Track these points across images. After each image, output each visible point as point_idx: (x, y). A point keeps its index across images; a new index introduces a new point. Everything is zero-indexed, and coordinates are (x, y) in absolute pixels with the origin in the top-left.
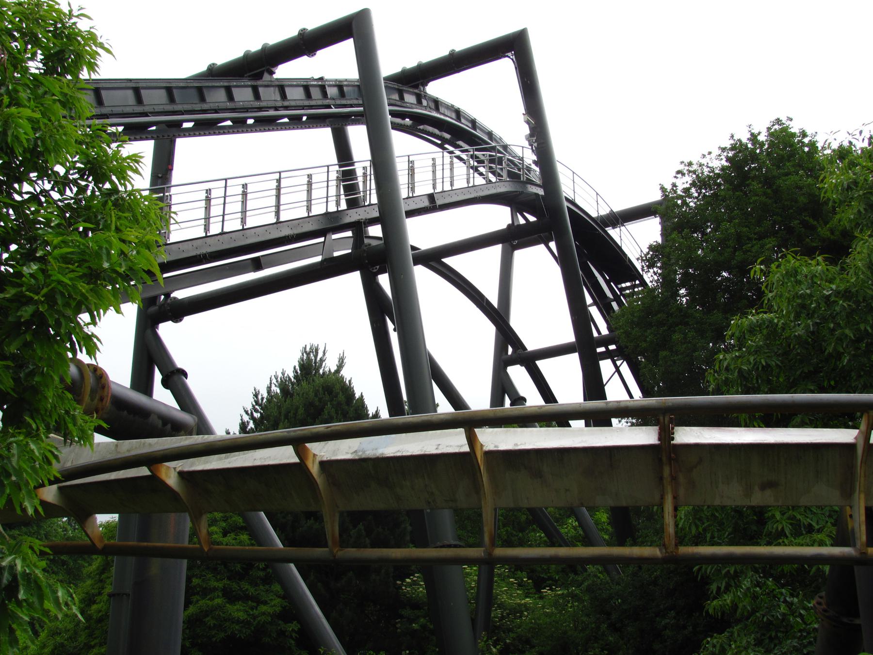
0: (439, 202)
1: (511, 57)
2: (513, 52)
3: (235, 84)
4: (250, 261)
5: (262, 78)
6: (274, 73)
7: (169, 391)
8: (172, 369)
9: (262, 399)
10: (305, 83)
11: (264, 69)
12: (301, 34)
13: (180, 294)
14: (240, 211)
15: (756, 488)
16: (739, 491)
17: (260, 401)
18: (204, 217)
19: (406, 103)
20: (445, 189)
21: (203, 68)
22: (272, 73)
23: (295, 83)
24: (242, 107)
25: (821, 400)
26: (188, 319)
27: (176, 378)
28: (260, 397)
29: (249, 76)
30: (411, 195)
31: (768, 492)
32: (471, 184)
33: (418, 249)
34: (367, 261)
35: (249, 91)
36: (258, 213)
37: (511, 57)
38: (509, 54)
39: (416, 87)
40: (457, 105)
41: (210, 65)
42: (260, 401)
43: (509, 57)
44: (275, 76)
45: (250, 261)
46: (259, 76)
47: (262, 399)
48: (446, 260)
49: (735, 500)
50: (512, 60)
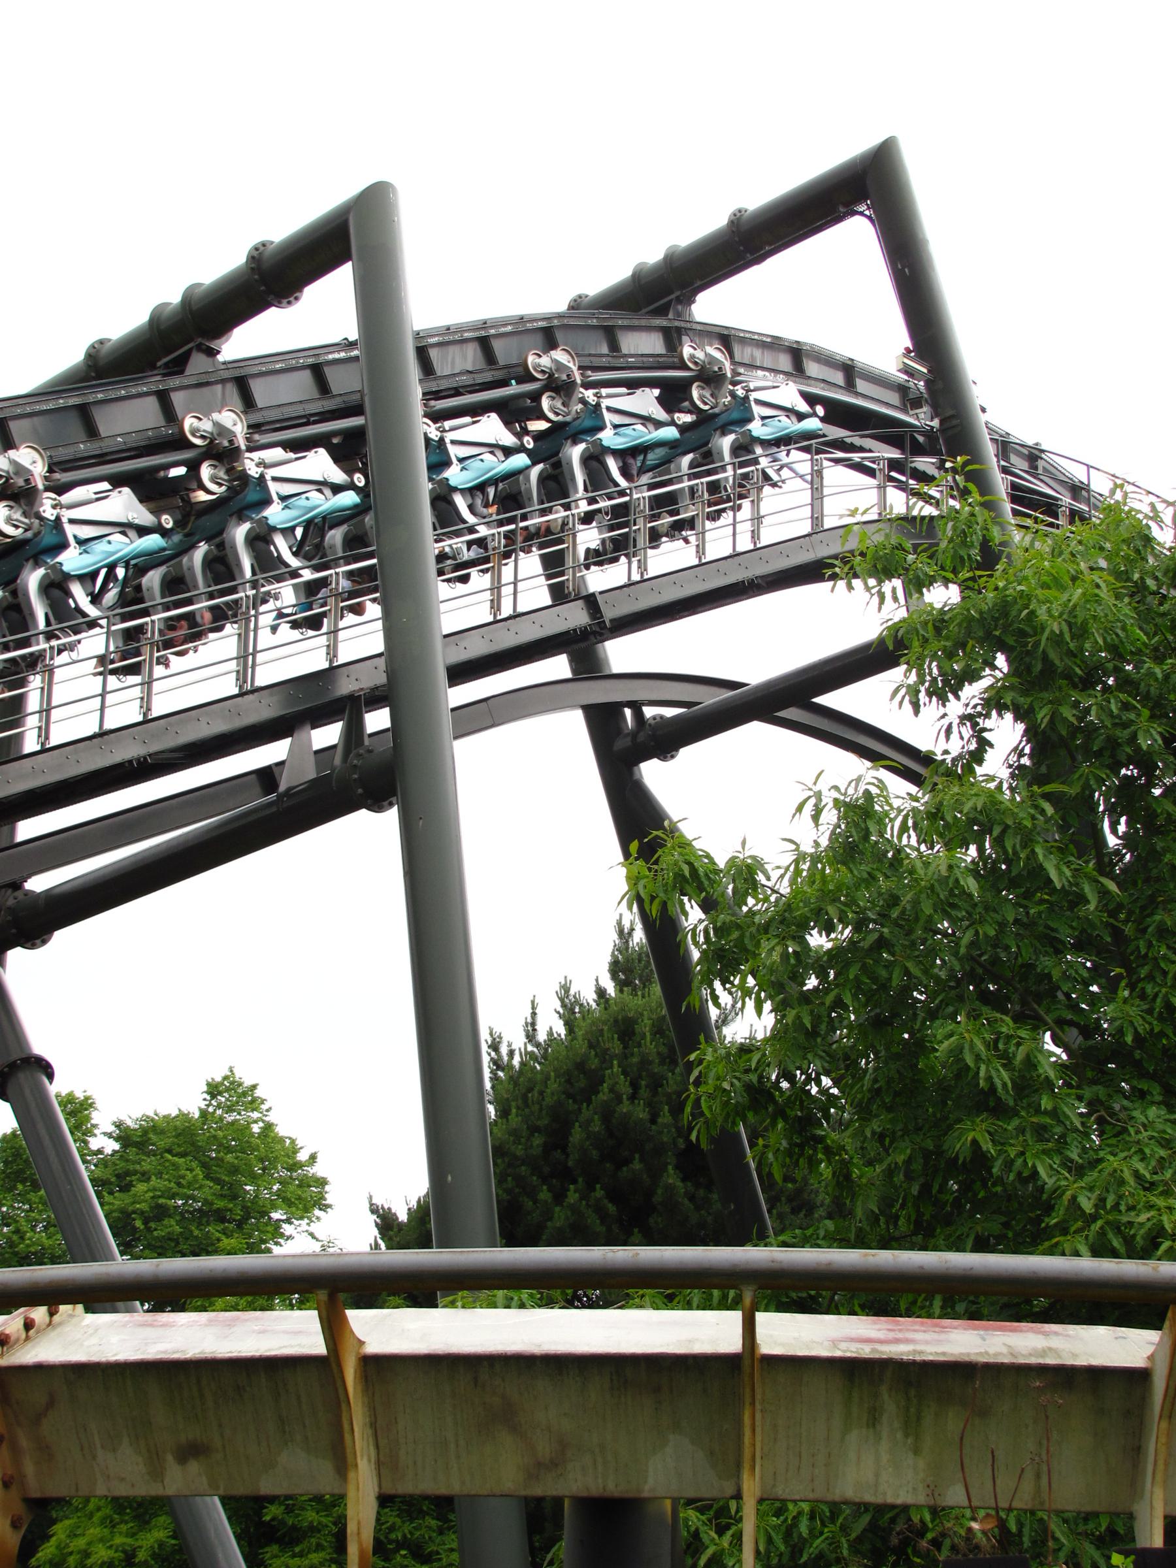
0: (610, 613)
1: (867, 213)
2: (869, 202)
3: (100, 396)
4: (254, 776)
5: (182, 372)
6: (218, 352)
7: (8, 1105)
8: (15, 1056)
9: (511, 1053)
10: (311, 361)
11: (190, 346)
12: (253, 258)
13: (38, 884)
14: (749, 517)
15: (170, 1458)
16: (137, 1464)
17: (506, 1058)
18: (235, 655)
19: (626, 356)
20: (740, 549)
21: (72, 356)
22: (212, 353)
23: (278, 366)
24: (124, 447)
25: (225, 1270)
26: (61, 936)
27: (22, 1077)
28: (504, 1050)
29: (166, 365)
30: (636, 577)
31: (194, 1467)
32: (506, 610)
33: (747, 685)
34: (360, 791)
35: (152, 403)
36: (223, 671)
37: (867, 213)
38: (862, 208)
39: (662, 311)
40: (791, 333)
41: (93, 346)
42: (506, 1058)
43: (861, 214)
44: (220, 358)
45: (254, 776)
46: (178, 366)
47: (511, 1053)
48: (826, 700)
49: (133, 1485)
50: (869, 218)
